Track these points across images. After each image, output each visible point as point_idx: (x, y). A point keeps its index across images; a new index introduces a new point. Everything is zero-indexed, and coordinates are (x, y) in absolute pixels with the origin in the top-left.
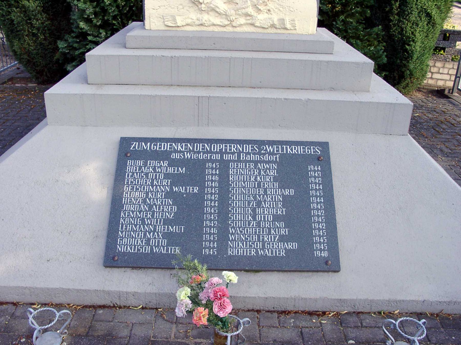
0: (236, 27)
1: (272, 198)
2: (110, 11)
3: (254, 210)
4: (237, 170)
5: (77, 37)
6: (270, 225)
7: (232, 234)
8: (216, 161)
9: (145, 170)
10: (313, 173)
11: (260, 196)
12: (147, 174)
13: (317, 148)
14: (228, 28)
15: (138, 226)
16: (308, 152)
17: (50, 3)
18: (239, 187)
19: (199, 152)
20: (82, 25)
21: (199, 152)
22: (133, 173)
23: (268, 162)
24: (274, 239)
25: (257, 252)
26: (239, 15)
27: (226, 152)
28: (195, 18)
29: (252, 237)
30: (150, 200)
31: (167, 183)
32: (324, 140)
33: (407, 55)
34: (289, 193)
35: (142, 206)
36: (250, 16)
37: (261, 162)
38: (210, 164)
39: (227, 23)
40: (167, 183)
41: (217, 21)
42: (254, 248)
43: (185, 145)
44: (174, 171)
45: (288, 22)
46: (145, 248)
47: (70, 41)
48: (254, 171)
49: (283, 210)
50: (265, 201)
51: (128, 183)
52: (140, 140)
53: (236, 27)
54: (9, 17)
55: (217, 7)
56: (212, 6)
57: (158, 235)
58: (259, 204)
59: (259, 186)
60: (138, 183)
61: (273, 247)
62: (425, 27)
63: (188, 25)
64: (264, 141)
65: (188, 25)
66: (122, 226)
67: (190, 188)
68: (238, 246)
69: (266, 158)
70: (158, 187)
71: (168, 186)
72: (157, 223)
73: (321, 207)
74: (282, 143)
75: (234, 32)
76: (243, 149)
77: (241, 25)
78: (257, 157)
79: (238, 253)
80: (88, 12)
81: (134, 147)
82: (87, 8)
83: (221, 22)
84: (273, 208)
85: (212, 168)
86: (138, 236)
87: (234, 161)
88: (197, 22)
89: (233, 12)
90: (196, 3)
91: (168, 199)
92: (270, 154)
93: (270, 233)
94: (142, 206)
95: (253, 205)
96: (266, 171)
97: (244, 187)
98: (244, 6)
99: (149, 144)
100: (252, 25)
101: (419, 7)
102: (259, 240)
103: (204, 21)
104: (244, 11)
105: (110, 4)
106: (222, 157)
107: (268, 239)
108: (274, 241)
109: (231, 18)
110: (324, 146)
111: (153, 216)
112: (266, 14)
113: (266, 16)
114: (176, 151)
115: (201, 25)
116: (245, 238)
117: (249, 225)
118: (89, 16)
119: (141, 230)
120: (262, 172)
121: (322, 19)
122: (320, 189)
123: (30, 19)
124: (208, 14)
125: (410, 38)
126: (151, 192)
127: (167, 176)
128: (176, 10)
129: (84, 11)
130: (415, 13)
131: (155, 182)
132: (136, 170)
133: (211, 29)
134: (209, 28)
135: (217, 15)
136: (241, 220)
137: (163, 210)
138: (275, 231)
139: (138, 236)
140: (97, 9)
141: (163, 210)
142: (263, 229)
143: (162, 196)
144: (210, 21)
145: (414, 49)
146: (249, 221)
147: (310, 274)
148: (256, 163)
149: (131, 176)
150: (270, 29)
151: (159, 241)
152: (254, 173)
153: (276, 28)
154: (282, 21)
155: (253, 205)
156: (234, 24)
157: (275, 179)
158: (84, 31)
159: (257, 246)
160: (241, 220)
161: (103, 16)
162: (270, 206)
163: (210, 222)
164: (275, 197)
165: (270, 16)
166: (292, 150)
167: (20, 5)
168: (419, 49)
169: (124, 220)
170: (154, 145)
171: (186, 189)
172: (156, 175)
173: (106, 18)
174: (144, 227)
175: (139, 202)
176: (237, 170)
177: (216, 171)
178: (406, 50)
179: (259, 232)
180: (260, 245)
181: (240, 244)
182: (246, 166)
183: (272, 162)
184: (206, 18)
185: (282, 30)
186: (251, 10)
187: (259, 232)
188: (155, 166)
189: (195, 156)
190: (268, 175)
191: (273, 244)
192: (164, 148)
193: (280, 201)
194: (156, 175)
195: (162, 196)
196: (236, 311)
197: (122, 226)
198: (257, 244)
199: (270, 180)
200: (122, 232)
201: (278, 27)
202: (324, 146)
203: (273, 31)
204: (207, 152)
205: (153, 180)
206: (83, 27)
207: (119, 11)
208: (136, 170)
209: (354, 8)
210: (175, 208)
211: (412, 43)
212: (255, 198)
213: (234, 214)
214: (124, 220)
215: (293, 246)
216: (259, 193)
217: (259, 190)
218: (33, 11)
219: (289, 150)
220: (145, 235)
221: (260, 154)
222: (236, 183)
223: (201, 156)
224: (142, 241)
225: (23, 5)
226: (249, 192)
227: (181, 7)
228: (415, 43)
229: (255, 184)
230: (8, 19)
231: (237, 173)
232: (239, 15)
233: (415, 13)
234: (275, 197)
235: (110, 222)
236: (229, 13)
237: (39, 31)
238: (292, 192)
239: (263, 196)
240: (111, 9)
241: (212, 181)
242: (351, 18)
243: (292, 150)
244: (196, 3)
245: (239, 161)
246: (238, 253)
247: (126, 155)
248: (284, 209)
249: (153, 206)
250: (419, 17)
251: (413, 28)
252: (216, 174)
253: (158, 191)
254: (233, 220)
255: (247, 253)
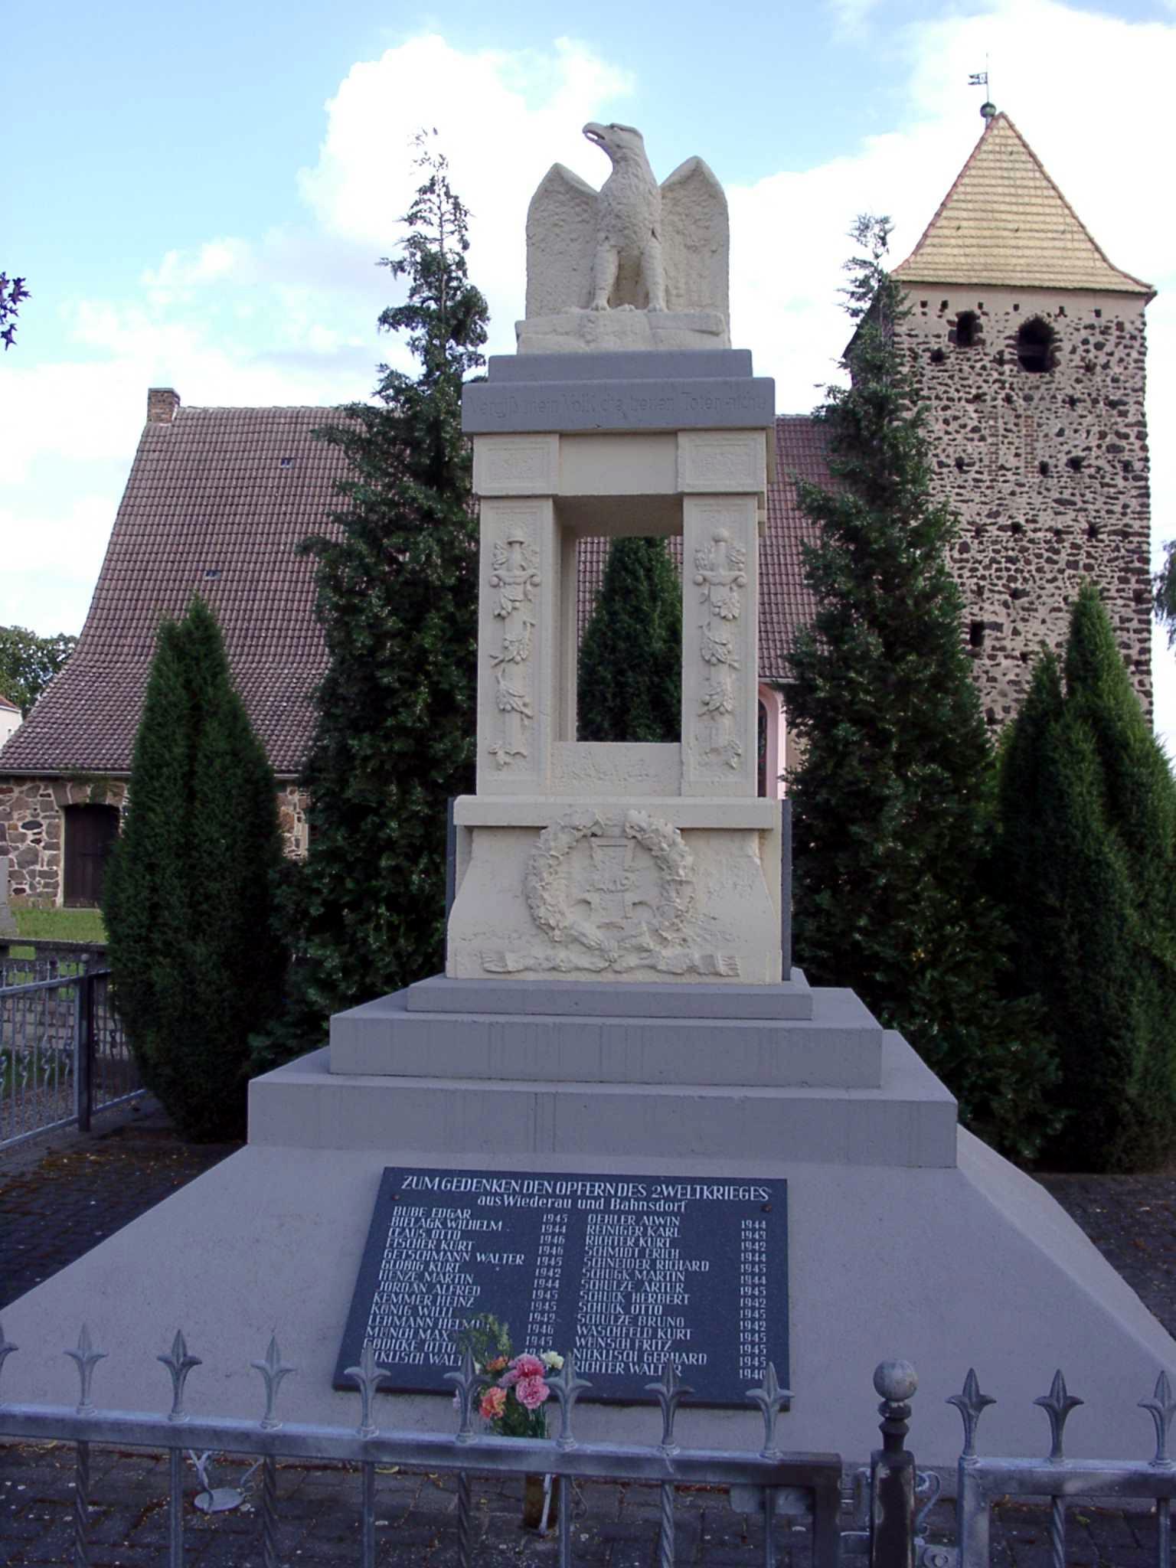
0: (620, 972)
1: (665, 1277)
2: (380, 964)
3: (628, 1296)
4: (601, 1228)
5: (295, 1025)
6: (656, 1323)
7: (582, 1336)
8: (562, 1211)
9: (426, 1224)
10: (749, 1234)
11: (641, 1272)
12: (429, 1232)
13: (764, 1191)
14: (604, 974)
15: (404, 1319)
16: (744, 1196)
17: (242, 947)
18: (602, 1257)
19: (531, 1196)
20: (313, 994)
21: (531, 1196)
22: (404, 1229)
23: (664, 1214)
24: (663, 1347)
25: (627, 1368)
26: (625, 949)
27: (583, 1196)
28: (541, 956)
29: (621, 1342)
30: (430, 1274)
31: (467, 1247)
32: (782, 1177)
33: (1115, 1062)
34: (700, 1267)
35: (415, 1286)
36: (647, 951)
37: (648, 1214)
38: (551, 1217)
39: (603, 964)
40: (467, 1247)
41: (585, 962)
42: (622, 1361)
43: (506, 1183)
44: (481, 1227)
45: (721, 962)
46: (415, 1356)
47: (279, 1033)
48: (634, 1229)
49: (683, 1298)
50: (650, 1282)
51: (391, 1245)
52: (420, 1172)
53: (620, 972)
54: (144, 977)
55: (584, 935)
56: (573, 932)
57: (441, 1335)
58: (638, 1286)
59: (642, 1254)
60: (411, 1245)
61: (659, 1360)
62: (1155, 993)
63: (527, 969)
64: (658, 1177)
65: (527, 969)
66: (374, 1320)
67: (508, 1257)
68: (592, 1356)
69: (661, 1206)
70: (449, 1254)
71: (467, 1252)
72: (440, 1313)
73: (760, 1292)
74: (693, 1181)
75: (618, 982)
76: (616, 1192)
77: (630, 969)
78: (642, 1205)
79: (590, 1369)
80: (328, 965)
81: (410, 1185)
82: (327, 957)
83: (592, 963)
84: (666, 1292)
85: (554, 1224)
86: (403, 1334)
87: (596, 1212)
88: (547, 965)
89: (614, 944)
90: (545, 927)
91: (465, 1273)
92: (668, 1199)
93: (655, 1335)
94: (415, 1286)
95: (627, 1287)
96: (658, 1229)
97: (611, 1257)
98: (633, 933)
99: (437, 1179)
100: (653, 967)
101: (1129, 943)
102: (632, 1348)
103: (558, 961)
104: (634, 941)
105: (380, 949)
106: (574, 1203)
107: (651, 1346)
108: (662, 1350)
109: (611, 954)
110: (778, 1187)
111: (434, 1302)
112: (679, 948)
113: (678, 950)
114: (487, 1193)
115: (554, 969)
116: (607, 1344)
117: (616, 1321)
118: (329, 975)
119: (410, 1326)
120: (650, 1231)
121: (885, 980)
122: (760, 1262)
123: (192, 982)
124: (566, 947)
125: (1118, 1019)
126: (434, 1261)
127: (467, 1235)
128: (507, 941)
129: (319, 963)
130: (1121, 957)
131: (443, 1245)
132: (409, 1224)
133: (572, 977)
134: (569, 975)
135: (584, 949)
136: (601, 1313)
137: (454, 1293)
138: (666, 1334)
139: (403, 1334)
140: (351, 960)
141: (454, 1293)
142: (642, 1328)
143: (454, 1269)
144: (570, 961)
145: (1129, 1046)
146: (616, 1316)
147: (730, 1413)
148: (639, 1215)
149: (400, 1234)
150: (687, 976)
151: (441, 1346)
152: (633, 1233)
153: (699, 974)
154: (709, 959)
155: (627, 1287)
156: (617, 967)
157: (674, 1243)
158: (316, 1008)
159: (628, 1357)
160: (601, 1313)
161: (363, 977)
162: (660, 1289)
163: (542, 1316)
164: (671, 1275)
165: (687, 950)
166: (712, 1193)
167: (174, 951)
168: (1144, 1046)
169: (379, 1309)
170: (447, 1182)
171: (501, 1259)
172: (446, 1234)
173: (368, 980)
174: (415, 1320)
175: (410, 1278)
176: (601, 1228)
177: (560, 1228)
178: (1112, 1052)
179: (635, 1334)
180: (634, 1356)
181: (595, 1353)
182: (619, 1220)
183: (672, 1214)
184: (563, 956)
185: (711, 977)
186: (647, 941)
187: (635, 1334)
188: (446, 1218)
189: (522, 1202)
190: (660, 1236)
191: (659, 1355)
192: (466, 1187)
193: (680, 1281)
194: (446, 1234)
195: (454, 1269)
196: (382, 763)
197: (374, 1320)
198: (628, 1354)
199: (664, 1244)
200: (373, 1328)
201: (702, 971)
202: (778, 1187)
203: (693, 979)
204: (548, 1196)
205: (439, 1241)
206: (314, 998)
207: (402, 965)
208: (409, 1224)
209: (960, 952)
210: (477, 1290)
211: (1123, 1032)
212: (632, 1275)
213: (588, 1301)
214: (379, 1309)
215: (697, 1360)
216: (641, 1266)
217: (641, 1262)
218: (201, 964)
219: (706, 1193)
220: (416, 1333)
221: (648, 1199)
222: (598, 1250)
223: (535, 1202)
224: (409, 1345)
225: (180, 950)
226: (620, 1266)
227: (515, 935)
228: (1133, 1031)
229: (634, 1251)
230: (142, 981)
231: (601, 1231)
232: (625, 949)
233: (1121, 957)
234: (671, 1275)
235: (353, 1310)
236: (606, 945)
237: (208, 1008)
238: (706, 1266)
239: (648, 1272)
240: (383, 960)
241: (552, 1245)
242: (956, 975)
243: (712, 1193)
244: (545, 927)
245: (607, 1210)
246: (590, 1369)
247: (393, 1198)
248: (686, 1296)
249: (435, 1285)
250: (1135, 968)
251: (1125, 995)
252: (560, 1234)
253: (447, 1261)
254: (586, 1313)
255: (607, 1370)
